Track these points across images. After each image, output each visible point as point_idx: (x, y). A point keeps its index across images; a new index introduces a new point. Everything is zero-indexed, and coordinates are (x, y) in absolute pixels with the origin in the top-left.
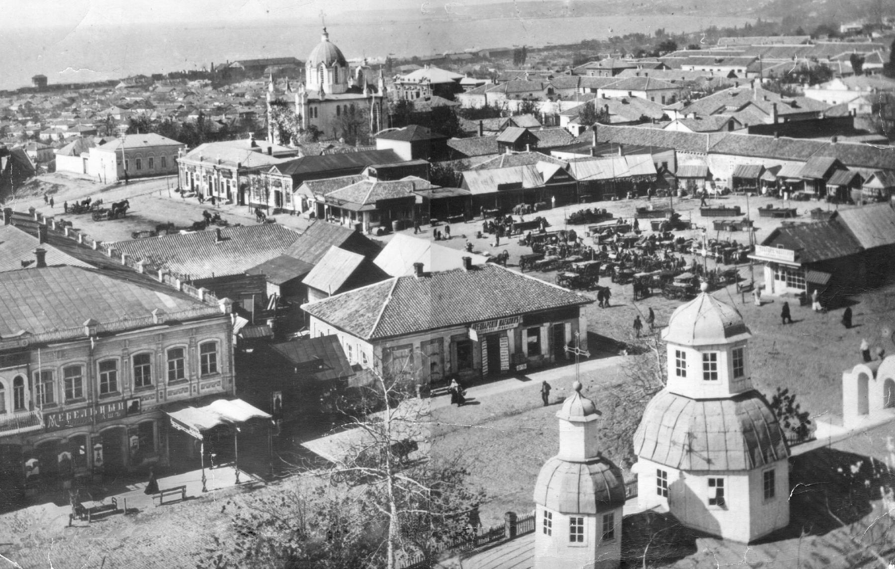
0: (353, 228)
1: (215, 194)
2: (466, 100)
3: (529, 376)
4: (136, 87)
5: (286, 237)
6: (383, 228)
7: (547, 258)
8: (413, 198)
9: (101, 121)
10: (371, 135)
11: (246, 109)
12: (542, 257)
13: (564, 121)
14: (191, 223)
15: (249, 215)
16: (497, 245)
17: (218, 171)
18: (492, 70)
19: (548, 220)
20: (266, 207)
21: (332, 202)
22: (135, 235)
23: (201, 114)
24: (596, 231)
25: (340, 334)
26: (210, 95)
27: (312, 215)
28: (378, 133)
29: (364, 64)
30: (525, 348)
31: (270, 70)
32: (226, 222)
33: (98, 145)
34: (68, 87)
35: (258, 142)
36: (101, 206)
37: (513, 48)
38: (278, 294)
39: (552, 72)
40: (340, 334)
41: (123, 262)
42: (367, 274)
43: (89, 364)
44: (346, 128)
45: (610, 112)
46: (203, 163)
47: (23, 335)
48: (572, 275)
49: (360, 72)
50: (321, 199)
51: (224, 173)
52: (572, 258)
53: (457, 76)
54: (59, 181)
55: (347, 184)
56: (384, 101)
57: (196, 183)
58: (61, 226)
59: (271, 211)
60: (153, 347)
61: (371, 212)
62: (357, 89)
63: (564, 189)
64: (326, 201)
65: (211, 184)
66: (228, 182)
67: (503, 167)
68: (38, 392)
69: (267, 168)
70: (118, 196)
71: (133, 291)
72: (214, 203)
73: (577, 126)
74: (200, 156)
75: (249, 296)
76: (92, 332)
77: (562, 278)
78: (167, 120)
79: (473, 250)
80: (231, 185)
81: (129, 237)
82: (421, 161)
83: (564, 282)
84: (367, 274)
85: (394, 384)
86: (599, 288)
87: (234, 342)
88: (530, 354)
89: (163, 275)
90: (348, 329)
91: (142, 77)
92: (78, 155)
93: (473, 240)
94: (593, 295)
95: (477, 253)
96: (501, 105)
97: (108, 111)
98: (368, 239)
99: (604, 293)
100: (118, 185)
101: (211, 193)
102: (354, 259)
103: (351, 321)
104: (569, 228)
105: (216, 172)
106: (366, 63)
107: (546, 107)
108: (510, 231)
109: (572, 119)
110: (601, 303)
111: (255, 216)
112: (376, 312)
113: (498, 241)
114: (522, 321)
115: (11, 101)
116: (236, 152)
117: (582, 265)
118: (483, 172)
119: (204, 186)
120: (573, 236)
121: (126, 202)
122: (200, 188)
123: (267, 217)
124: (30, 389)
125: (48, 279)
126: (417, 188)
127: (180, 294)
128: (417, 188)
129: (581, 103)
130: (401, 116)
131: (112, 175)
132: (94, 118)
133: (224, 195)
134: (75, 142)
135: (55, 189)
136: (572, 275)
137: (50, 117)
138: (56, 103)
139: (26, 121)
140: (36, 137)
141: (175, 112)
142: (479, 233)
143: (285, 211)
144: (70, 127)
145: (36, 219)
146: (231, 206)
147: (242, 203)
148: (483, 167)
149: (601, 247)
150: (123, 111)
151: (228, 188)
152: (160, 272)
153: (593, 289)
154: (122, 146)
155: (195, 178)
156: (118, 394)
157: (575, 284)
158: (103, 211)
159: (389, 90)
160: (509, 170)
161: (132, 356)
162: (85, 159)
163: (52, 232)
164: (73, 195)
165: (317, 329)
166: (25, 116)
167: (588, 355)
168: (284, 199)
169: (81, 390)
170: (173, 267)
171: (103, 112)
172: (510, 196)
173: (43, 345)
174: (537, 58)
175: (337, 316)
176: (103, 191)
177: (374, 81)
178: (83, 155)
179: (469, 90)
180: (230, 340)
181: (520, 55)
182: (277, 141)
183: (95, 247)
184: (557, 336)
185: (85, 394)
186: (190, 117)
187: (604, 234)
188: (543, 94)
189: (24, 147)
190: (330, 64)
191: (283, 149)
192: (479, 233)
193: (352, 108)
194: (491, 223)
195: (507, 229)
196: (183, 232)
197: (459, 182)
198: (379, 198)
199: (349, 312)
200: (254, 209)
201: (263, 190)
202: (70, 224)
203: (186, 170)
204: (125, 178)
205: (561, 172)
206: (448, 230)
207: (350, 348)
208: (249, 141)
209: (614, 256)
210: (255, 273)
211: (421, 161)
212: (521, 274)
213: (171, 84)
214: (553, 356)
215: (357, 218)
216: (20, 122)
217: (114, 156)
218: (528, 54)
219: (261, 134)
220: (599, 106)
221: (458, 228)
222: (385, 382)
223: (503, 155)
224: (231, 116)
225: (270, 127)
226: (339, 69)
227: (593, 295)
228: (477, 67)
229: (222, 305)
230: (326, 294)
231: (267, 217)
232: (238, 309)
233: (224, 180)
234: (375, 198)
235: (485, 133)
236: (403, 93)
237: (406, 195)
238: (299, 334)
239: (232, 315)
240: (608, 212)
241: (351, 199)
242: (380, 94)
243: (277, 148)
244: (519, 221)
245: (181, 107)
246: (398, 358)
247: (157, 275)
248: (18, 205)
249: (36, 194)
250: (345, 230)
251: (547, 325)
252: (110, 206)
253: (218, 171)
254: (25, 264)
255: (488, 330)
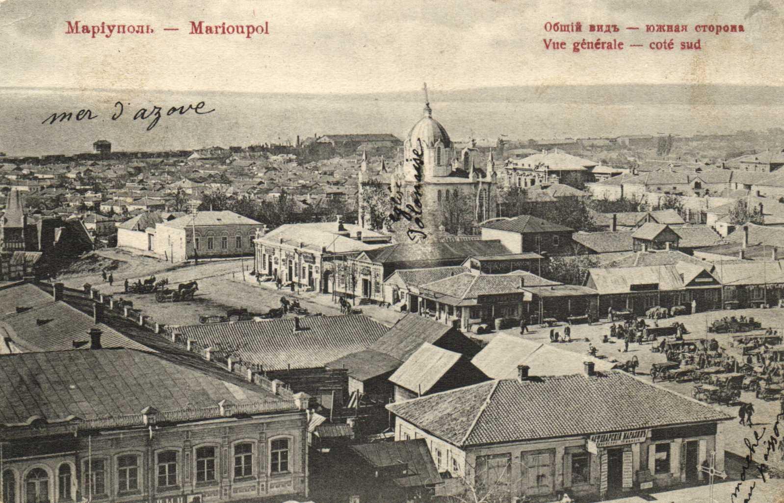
0: (450, 325)
1: (295, 279)
2: (598, 190)
3: (654, 495)
4: (212, 159)
5: (372, 330)
6: (484, 326)
7: (683, 367)
8: (522, 294)
9: (170, 195)
10: (476, 224)
11: (335, 189)
12: (677, 367)
13: (711, 219)
14: (267, 310)
15: (332, 304)
16: (626, 351)
17: (300, 254)
18: (632, 159)
19: (686, 326)
20: (352, 297)
21: (427, 295)
22: (204, 319)
23: (283, 192)
24: (741, 342)
25: (429, 439)
26: (294, 171)
27: (404, 308)
28: (484, 222)
29: (471, 146)
30: (652, 465)
31: (363, 147)
32: (306, 310)
33: (166, 221)
34: (135, 155)
35: (346, 226)
36: (166, 287)
37: (657, 135)
38: (361, 391)
39: (701, 164)
40: (429, 439)
41: (189, 348)
42: (463, 375)
43: (146, 454)
44: (447, 215)
45: (764, 212)
46: (283, 245)
47: (73, 420)
48: (711, 388)
49: (466, 154)
50: (415, 291)
51: (306, 257)
52: (713, 369)
53: (589, 163)
54: (121, 257)
55: (445, 276)
56: (493, 187)
57: (274, 266)
58: (119, 307)
59: (357, 301)
60: (220, 440)
61: (472, 308)
62: (461, 173)
63: (703, 295)
64: (421, 294)
65: (290, 269)
66: (310, 267)
67: (637, 266)
68: (87, 481)
69: (355, 254)
70: (186, 276)
71: (194, 378)
72: (293, 289)
73: (726, 225)
74: (280, 238)
75: (328, 392)
76: (151, 421)
77: (699, 391)
78: (244, 196)
79: (597, 354)
80: (314, 270)
81: (197, 322)
82: (534, 255)
83: (702, 396)
84: (463, 375)
85: (488, 495)
86: (740, 404)
87: (309, 440)
88: (657, 471)
89: (233, 364)
90: (438, 433)
91: (218, 148)
92: (143, 231)
93: (597, 343)
94: (735, 411)
95: (602, 357)
96: (639, 198)
97: (179, 183)
98: (465, 338)
99: (746, 410)
100: (186, 265)
101: (291, 279)
102: (449, 358)
103: (442, 425)
104: (711, 336)
105: (297, 256)
106: (474, 145)
107: (691, 202)
108: (641, 337)
109: (721, 217)
110: (742, 420)
111: (339, 306)
112: (471, 417)
113: (627, 346)
114: (650, 435)
115: (68, 168)
116: (320, 236)
117: (723, 377)
118: (615, 271)
119: (283, 270)
120: (715, 345)
121: (195, 283)
122: (279, 272)
123: (353, 307)
124: (78, 477)
125: (102, 360)
126: (530, 286)
127: (251, 385)
128: (525, 284)
129: (732, 200)
130: (514, 205)
131: (180, 253)
132: (163, 192)
133: (305, 281)
134: (140, 216)
135: (115, 265)
136: (711, 388)
137: (113, 187)
138: (120, 173)
139: (86, 190)
140: (96, 208)
141: (254, 188)
142: (606, 336)
143: (374, 302)
144: (135, 200)
145: (92, 296)
146: (312, 293)
147: (326, 291)
148: (614, 265)
149: (746, 357)
150: (196, 185)
151: (310, 273)
152: (229, 361)
153: (734, 405)
154: (192, 223)
155: (273, 261)
156: (177, 488)
157: (715, 398)
158: (168, 292)
159: (499, 175)
160: (642, 269)
161: (270, 440)
162: (150, 235)
163: (110, 311)
164: (135, 273)
165: (403, 431)
166: (84, 184)
167: (724, 476)
168: (373, 288)
169: (135, 481)
170: (245, 356)
171: (173, 185)
172: (643, 298)
173: (96, 432)
174: (684, 149)
175: (428, 418)
176: (169, 270)
177: (482, 165)
178: (149, 230)
179: (602, 179)
180: (304, 438)
181: (665, 144)
182: (368, 226)
183: (157, 330)
184: (690, 453)
185: (141, 487)
186: (271, 195)
187: (750, 345)
188: (689, 188)
189: (82, 218)
190: (433, 145)
191: (375, 234)
192: (606, 336)
193: (456, 194)
194: (620, 327)
195: (639, 334)
196: (258, 319)
197: (582, 279)
198: (482, 293)
199: (440, 415)
200: (338, 298)
201: (349, 278)
202: (130, 303)
203: (264, 252)
204: (195, 258)
205: (704, 274)
206: (568, 331)
207: (439, 454)
208: (336, 224)
209: (761, 370)
210: (337, 367)
211: (534, 255)
212: (653, 385)
213: (252, 157)
214: (684, 476)
215: (455, 313)
216: (78, 191)
217: (183, 234)
218: (674, 144)
219: (351, 218)
220: (753, 203)
221: (580, 331)
222: (477, 493)
223: (639, 253)
224: (316, 197)
225: (360, 210)
226: (443, 150)
227: (735, 411)
228: (614, 155)
229: (298, 400)
230: (416, 395)
231: (353, 307)
232: (313, 405)
233: (306, 265)
234: (477, 294)
235: (618, 228)
236: (515, 179)
237: (514, 291)
238: (382, 436)
239: (308, 411)
240: (756, 320)
241: (449, 293)
242: (488, 179)
243: (367, 233)
244: (653, 326)
245: (261, 183)
246: (494, 467)
247: (226, 363)
248: (73, 282)
249: (93, 270)
250: (441, 326)
251: (680, 440)
252: (176, 287)
253: (300, 254)
254: (77, 345)
255: (610, 443)
